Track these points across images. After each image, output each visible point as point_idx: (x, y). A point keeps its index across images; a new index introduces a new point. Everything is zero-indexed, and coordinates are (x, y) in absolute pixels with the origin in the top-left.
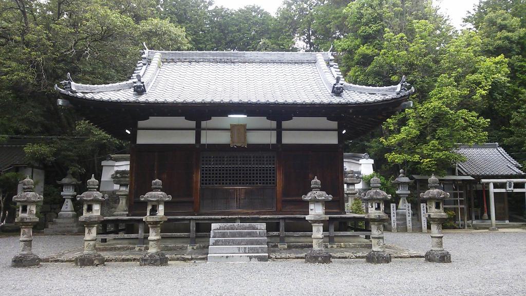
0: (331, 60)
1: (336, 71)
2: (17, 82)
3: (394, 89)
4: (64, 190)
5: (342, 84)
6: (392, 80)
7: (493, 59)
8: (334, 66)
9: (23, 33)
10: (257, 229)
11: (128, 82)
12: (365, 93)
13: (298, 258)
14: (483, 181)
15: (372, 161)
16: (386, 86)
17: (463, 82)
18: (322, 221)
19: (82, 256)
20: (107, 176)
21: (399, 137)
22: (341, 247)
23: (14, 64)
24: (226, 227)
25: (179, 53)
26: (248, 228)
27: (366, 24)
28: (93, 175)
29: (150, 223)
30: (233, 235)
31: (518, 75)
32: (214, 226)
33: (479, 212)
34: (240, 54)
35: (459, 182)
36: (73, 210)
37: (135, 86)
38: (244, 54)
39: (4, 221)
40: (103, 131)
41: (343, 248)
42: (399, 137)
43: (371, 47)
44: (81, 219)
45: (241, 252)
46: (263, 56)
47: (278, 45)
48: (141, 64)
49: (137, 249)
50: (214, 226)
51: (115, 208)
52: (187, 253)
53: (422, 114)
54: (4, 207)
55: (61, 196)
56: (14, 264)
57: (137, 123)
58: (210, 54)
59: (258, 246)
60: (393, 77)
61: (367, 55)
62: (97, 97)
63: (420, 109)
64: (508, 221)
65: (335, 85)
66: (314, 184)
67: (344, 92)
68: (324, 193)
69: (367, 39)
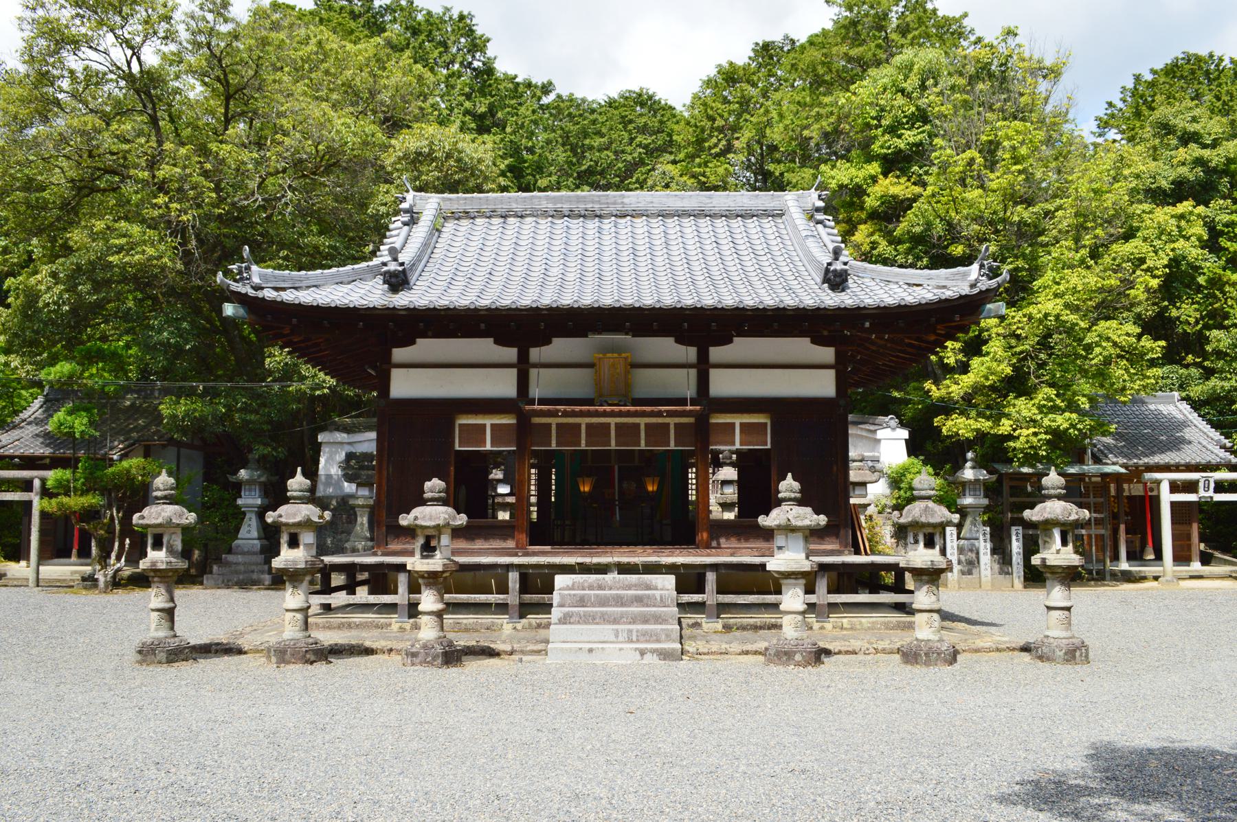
0: (818, 210)
1: (829, 234)
2: (143, 267)
3: (965, 275)
4: (243, 493)
5: (845, 264)
6: (950, 254)
7: (1169, 209)
8: (827, 222)
9: (152, 165)
10: (656, 589)
11: (371, 263)
12: (897, 283)
13: (747, 653)
14: (1148, 476)
15: (904, 434)
16: (946, 268)
17: (1107, 260)
18: (803, 575)
19: (280, 643)
20: (330, 464)
21: (968, 380)
22: (842, 628)
23: (135, 229)
24: (586, 585)
25: (480, 199)
26: (636, 586)
27: (893, 130)
28: (299, 469)
29: (422, 575)
30: (603, 602)
31: (1224, 242)
32: (560, 580)
33: (1138, 544)
34: (615, 197)
35: (1094, 479)
36: (263, 535)
37: (386, 272)
38: (623, 196)
39: (123, 559)
40: (320, 370)
41: (846, 629)
42: (968, 380)
43: (903, 180)
44: (277, 563)
45: (621, 639)
46: (665, 200)
47: (694, 176)
48: (399, 224)
49: (395, 627)
50: (560, 580)
51: (349, 533)
52: (503, 637)
53: (1018, 328)
54: (121, 530)
55: (238, 507)
56: (139, 657)
57: (390, 354)
58: (547, 198)
59: (659, 627)
60: (952, 248)
61: (894, 197)
62: (306, 297)
63: (1013, 317)
64: (1199, 564)
65: (829, 264)
66: (787, 491)
67: (850, 281)
68: (809, 510)
69: (895, 163)
